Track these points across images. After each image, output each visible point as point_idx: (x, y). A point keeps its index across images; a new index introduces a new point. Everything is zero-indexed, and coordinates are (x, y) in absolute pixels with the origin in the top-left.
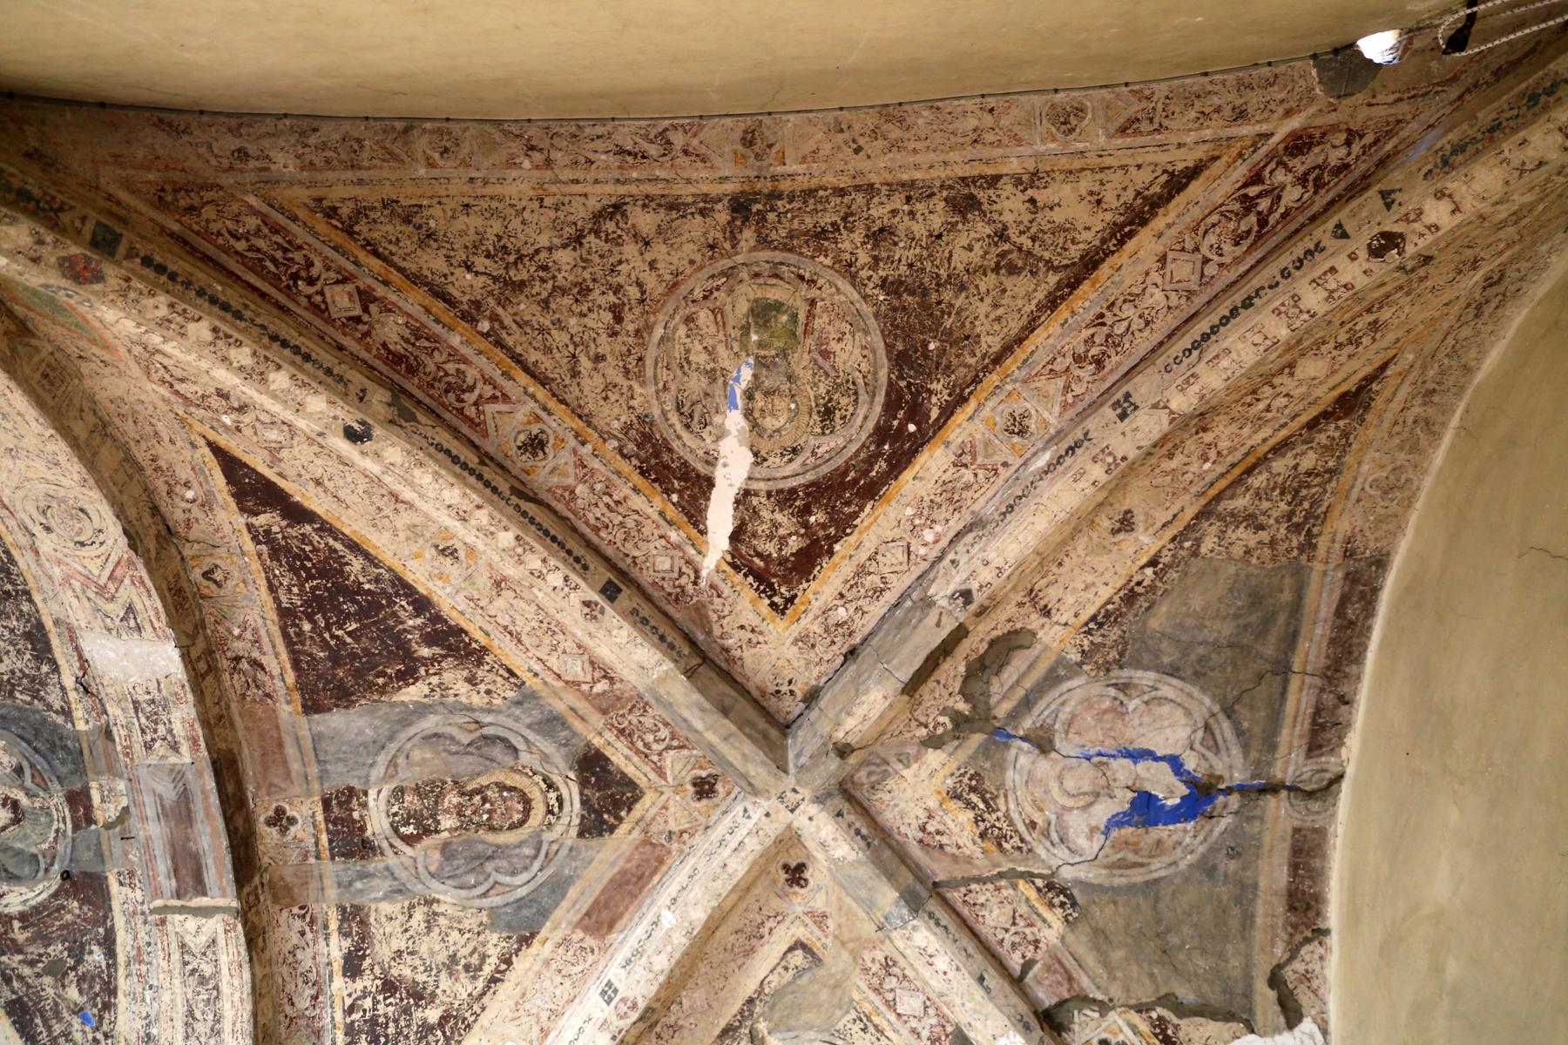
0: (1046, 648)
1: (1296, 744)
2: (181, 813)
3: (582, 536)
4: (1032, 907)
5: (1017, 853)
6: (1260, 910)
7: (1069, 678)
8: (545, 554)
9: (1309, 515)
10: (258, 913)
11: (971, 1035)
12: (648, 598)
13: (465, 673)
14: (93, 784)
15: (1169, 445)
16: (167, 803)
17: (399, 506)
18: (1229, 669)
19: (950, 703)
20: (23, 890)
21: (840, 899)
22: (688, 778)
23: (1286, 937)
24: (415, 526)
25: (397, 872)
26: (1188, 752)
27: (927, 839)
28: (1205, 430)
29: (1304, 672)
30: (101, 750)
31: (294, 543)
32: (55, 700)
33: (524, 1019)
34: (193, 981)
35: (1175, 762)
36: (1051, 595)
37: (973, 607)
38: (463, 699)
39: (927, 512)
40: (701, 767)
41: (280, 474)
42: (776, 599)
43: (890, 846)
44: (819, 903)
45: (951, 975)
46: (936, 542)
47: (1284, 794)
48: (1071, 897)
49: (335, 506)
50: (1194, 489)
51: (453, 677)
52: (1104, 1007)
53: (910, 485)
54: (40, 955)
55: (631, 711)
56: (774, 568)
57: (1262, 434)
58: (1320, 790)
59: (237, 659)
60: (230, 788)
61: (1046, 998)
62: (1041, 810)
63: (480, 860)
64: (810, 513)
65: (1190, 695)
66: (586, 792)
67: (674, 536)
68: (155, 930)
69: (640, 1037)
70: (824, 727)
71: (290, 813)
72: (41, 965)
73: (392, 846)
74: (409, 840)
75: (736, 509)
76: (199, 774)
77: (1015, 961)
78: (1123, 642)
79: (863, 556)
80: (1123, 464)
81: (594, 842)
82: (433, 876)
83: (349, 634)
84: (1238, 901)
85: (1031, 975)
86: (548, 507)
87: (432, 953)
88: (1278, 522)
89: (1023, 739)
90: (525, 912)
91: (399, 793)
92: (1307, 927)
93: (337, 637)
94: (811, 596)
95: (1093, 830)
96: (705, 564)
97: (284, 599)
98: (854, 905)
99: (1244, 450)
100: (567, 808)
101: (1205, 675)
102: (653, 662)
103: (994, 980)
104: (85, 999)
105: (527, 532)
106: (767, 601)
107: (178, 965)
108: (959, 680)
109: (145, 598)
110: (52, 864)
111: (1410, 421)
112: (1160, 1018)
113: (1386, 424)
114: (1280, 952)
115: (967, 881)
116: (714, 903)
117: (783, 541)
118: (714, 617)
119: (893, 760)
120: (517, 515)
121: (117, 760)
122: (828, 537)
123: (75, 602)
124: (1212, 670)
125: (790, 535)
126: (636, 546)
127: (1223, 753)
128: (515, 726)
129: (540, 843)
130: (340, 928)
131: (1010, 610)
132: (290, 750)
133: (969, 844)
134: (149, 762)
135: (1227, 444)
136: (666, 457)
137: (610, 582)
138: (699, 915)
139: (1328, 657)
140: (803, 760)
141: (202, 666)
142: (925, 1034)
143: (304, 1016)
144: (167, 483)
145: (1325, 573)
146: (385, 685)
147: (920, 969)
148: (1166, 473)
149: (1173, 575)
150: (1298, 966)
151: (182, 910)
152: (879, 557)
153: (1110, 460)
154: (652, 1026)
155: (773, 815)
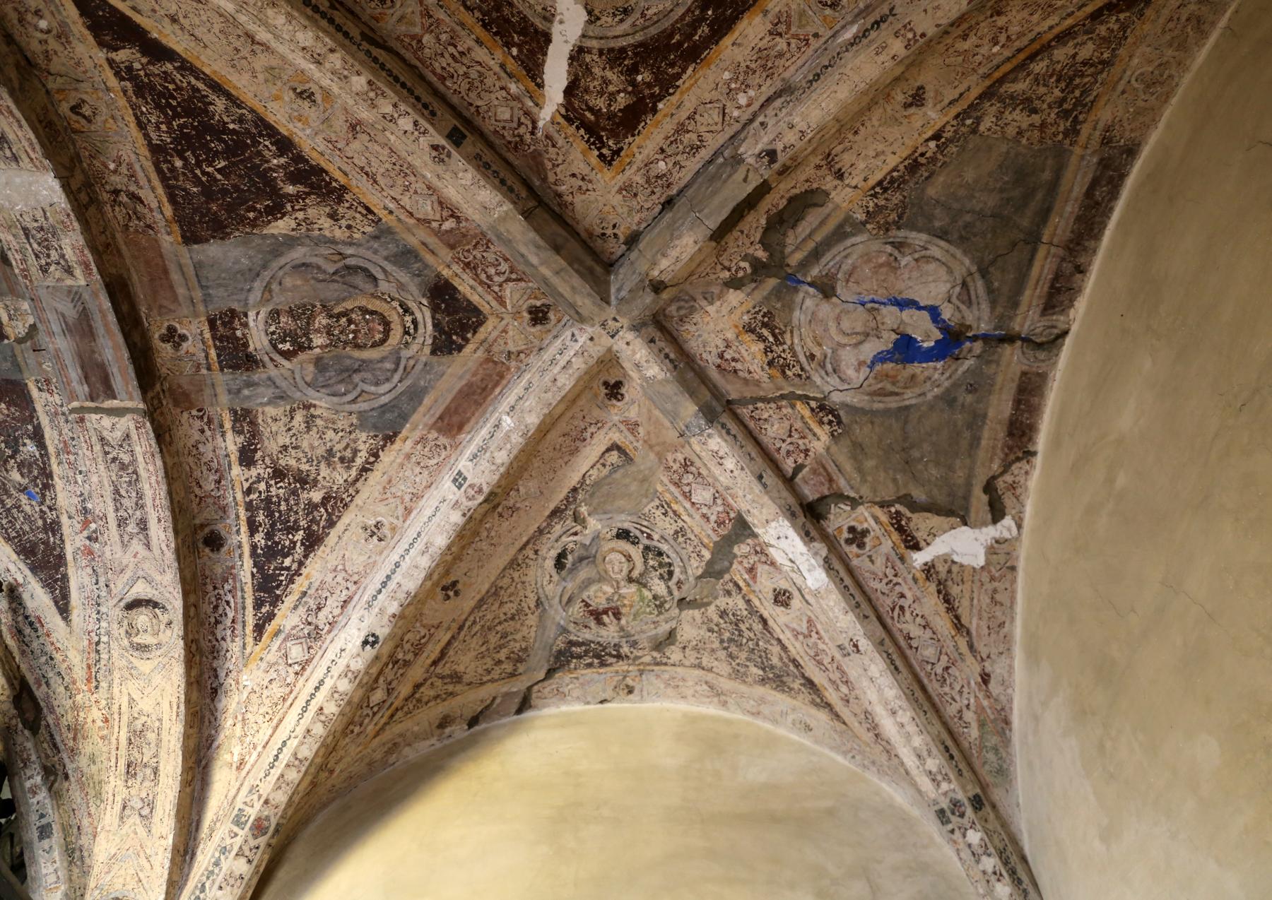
0: (837, 207)
1: (1034, 303)
2: (83, 328)
3: (430, 84)
4: (806, 423)
5: (797, 380)
6: (986, 434)
7: (854, 235)
8: (396, 99)
9: (1078, 102)
10: (162, 413)
11: (749, 519)
12: (491, 145)
13: (327, 209)
15: (965, 26)
16: (70, 321)
17: (256, 47)
18: (989, 236)
19: (751, 251)
21: (649, 411)
22: (525, 307)
23: (1002, 456)
24: (272, 68)
25: (278, 382)
26: (946, 304)
27: (724, 365)
28: (999, 13)
29: (1051, 243)
31: (157, 81)
33: (391, 500)
35: (934, 312)
36: (846, 160)
37: (776, 166)
38: (327, 233)
39: (743, 76)
40: (536, 298)
41: (134, 8)
42: (605, 151)
43: (693, 369)
44: (633, 414)
45: (736, 473)
46: (749, 105)
47: (1019, 343)
48: (837, 417)
49: (193, 44)
50: (981, 71)
51: (317, 213)
52: (854, 503)
53: (728, 51)
55: (475, 246)
56: (603, 122)
57: (1050, 22)
58: (1048, 342)
59: (116, 192)
60: (125, 308)
61: (810, 494)
62: (820, 345)
63: (349, 372)
64: (638, 73)
65: (953, 256)
66: (438, 316)
67: (513, 88)
68: (75, 425)
69: (485, 515)
70: (643, 266)
71: (180, 331)
73: (272, 359)
74: (287, 355)
75: (570, 65)
76: (95, 295)
77: (789, 465)
78: (903, 205)
79: (683, 115)
80: (922, 41)
81: (445, 359)
82: (309, 385)
83: (219, 171)
84: (970, 426)
85: (800, 476)
86: (397, 54)
87: (312, 448)
88: (1050, 107)
89: (810, 285)
90: (388, 416)
91: (275, 315)
92: (1020, 449)
93: (208, 174)
94: (635, 150)
95: (861, 364)
96: (542, 115)
97: (153, 135)
98: (661, 416)
99: (1031, 36)
100: (421, 330)
101: (968, 239)
102: (494, 202)
103: (770, 478)
104: (27, 481)
105: (378, 77)
106: (596, 153)
107: (101, 455)
108: (760, 231)
109: (15, 125)
111: (1183, 18)
112: (897, 512)
113: (1162, 20)
114: (996, 466)
115: (755, 400)
116: (546, 411)
117: (612, 97)
118: (549, 165)
119: (699, 297)
120: (369, 60)
121: (17, 283)
122: (652, 95)
124: (975, 236)
125: (619, 92)
126: (479, 95)
127: (975, 307)
128: (375, 258)
129: (399, 359)
130: (233, 428)
131: (809, 171)
132: (175, 276)
133: (759, 370)
134: (46, 284)
135: (1018, 29)
136: (506, 11)
137: (455, 128)
138: (533, 420)
139: (1072, 232)
140: (623, 293)
141: (83, 197)
142: (713, 518)
143: (210, 496)
144: (15, 9)
145: (1082, 157)
146: (256, 219)
147: (713, 468)
148: (959, 53)
149: (953, 149)
150: (1008, 478)
151: (97, 410)
152: (697, 117)
153: (910, 35)
154: (495, 507)
155: (596, 339)
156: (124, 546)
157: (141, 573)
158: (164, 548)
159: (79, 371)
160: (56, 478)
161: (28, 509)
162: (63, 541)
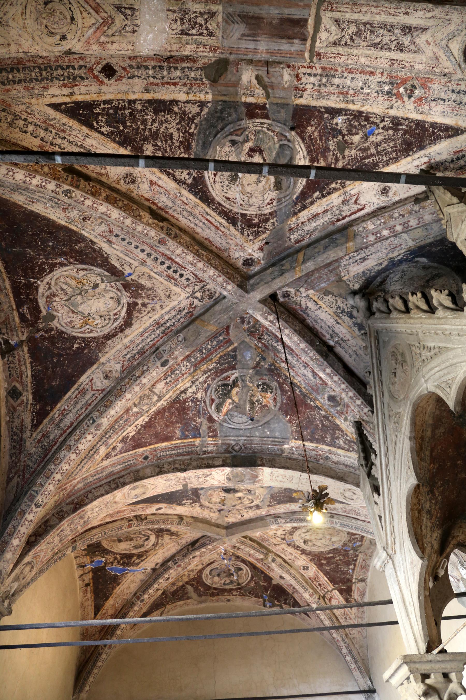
14: (243, 99)
16: (247, 32)
20: (298, 157)
30: (223, 88)
32: (194, 109)
34: (358, 41)
54: (333, 155)
72: (338, 155)
104: (360, 132)
107: (346, 49)
110: (286, 137)
123: (115, 46)
151: (314, 41)
156: (418, 51)
157: (444, 43)
158: (430, 14)
159: (283, 41)
160: (363, 109)
161: (380, 138)
162: (407, 119)
